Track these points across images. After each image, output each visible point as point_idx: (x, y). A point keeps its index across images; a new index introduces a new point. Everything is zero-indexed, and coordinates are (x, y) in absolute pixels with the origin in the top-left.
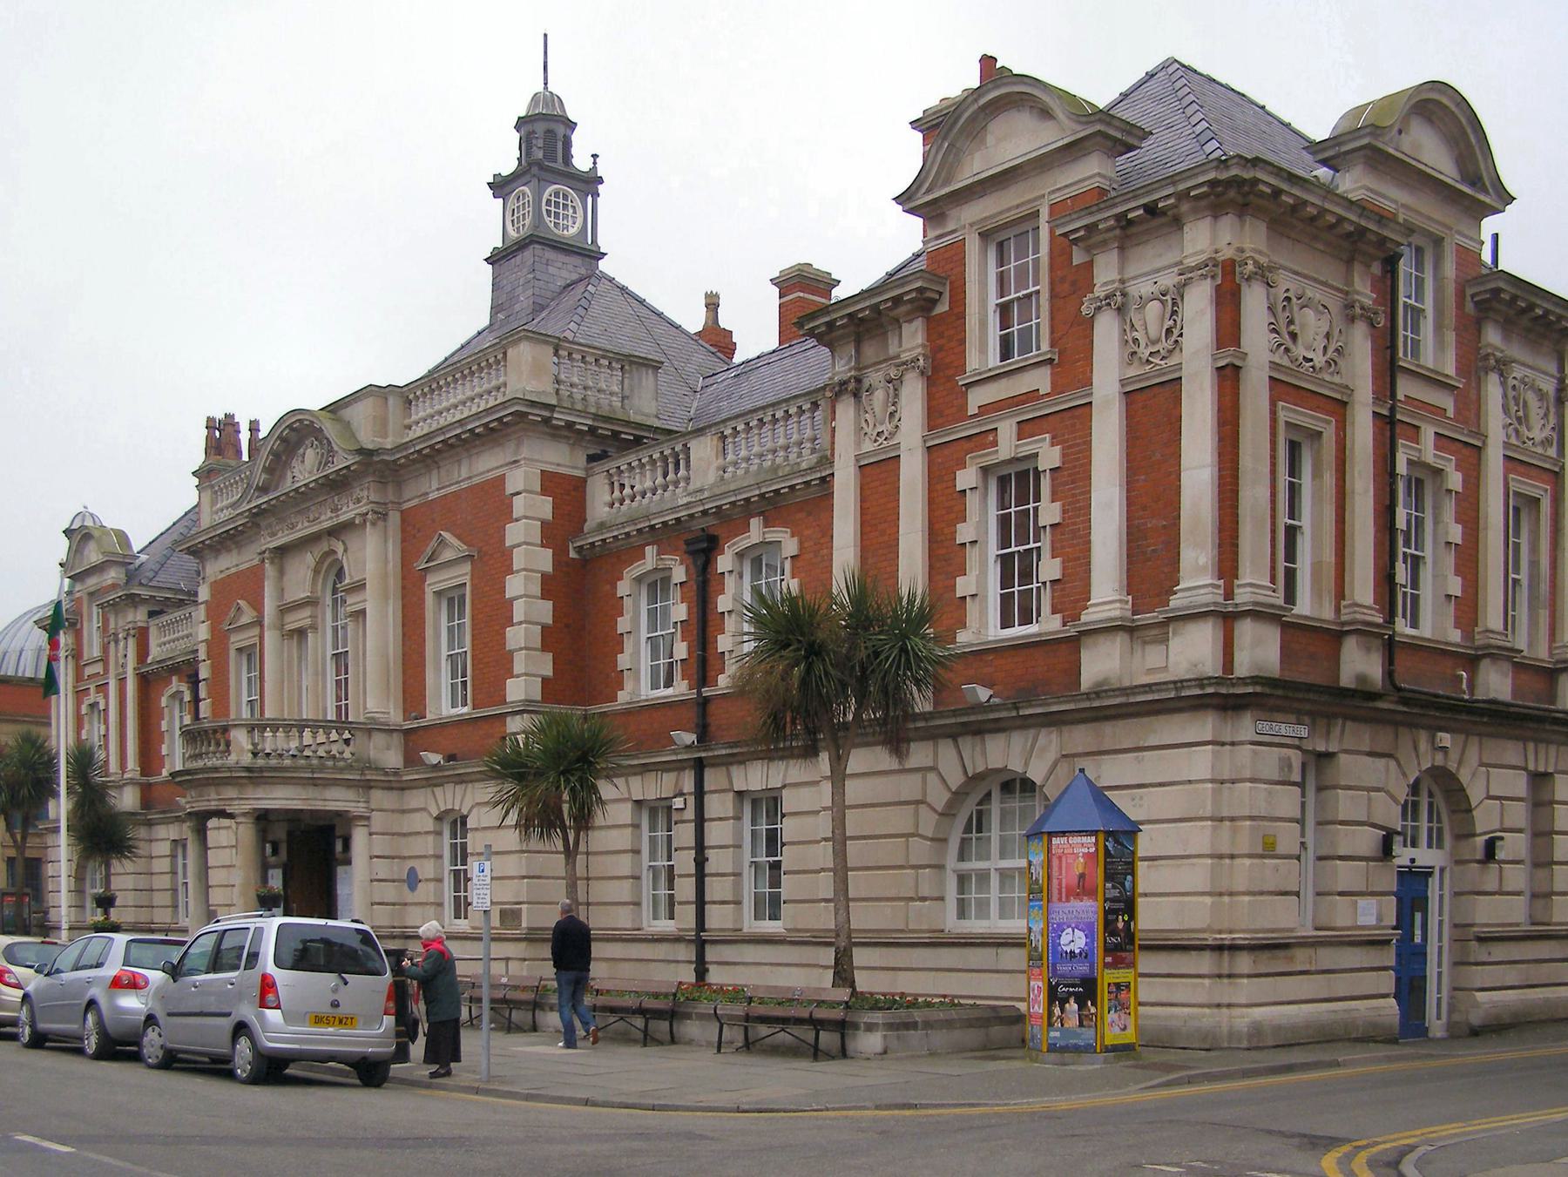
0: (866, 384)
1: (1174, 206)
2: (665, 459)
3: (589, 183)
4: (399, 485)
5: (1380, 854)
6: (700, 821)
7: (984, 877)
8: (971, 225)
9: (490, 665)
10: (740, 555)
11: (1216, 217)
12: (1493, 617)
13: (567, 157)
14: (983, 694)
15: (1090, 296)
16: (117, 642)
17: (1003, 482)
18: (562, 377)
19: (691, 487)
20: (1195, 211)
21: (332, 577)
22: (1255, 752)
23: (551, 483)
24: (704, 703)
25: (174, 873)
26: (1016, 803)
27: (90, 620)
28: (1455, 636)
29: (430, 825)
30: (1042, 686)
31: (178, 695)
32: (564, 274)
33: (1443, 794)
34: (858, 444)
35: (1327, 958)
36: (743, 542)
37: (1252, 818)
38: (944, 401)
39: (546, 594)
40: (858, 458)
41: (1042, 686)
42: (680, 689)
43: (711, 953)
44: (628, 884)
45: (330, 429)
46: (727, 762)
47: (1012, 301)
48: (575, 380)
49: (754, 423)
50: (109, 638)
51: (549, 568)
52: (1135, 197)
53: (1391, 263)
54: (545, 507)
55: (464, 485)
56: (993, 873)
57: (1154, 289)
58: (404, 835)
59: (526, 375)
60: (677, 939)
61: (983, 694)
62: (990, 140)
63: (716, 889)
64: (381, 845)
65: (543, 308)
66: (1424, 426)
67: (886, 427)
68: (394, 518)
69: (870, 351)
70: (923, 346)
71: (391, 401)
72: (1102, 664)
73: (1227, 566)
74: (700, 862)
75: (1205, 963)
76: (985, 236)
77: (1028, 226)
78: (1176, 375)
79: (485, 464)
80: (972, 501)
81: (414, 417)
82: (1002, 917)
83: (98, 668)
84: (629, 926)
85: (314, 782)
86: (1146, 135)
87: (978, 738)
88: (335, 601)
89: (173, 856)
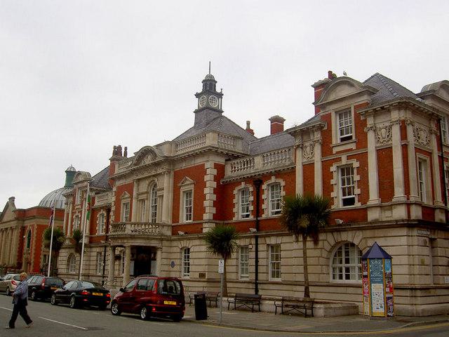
3: (220, 95)
4: (174, 165)
9: (199, 210)
10: (268, 185)
13: (215, 89)
14: (341, 222)
17: (343, 170)
24: (258, 222)
29: (179, 250)
35: (439, 292)
38: (73, 209)
41: (356, 219)
42: (251, 218)
43: (259, 287)
44: (179, 260)
45: (157, 151)
53: (439, 121)
54: (215, 172)
59: (211, 140)
60: (249, 283)
61: (341, 222)
63: (261, 269)
67: (310, 156)
68: (172, 173)
69: (305, 138)
72: (372, 215)
73: (407, 191)
74: (257, 262)
75: (408, 293)
77: (348, 111)
79: (199, 161)
80: (335, 174)
85: (148, 239)
86: (378, 91)
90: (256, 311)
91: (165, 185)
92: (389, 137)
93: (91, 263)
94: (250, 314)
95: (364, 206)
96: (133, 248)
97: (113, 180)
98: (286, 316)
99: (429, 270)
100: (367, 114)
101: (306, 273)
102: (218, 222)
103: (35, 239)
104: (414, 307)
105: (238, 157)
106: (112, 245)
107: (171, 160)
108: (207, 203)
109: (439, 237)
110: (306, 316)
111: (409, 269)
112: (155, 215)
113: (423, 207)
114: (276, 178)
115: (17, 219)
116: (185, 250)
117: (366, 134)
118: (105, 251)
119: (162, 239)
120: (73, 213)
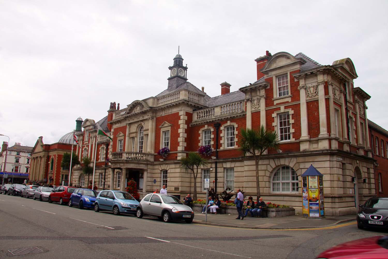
0: (253, 99)
1: (316, 73)
2: (204, 112)
3: (186, 69)
4: (156, 113)
5: (352, 181)
6: (216, 173)
7: (278, 184)
8: (274, 75)
10: (203, 131)
11: (323, 75)
12: (361, 142)
13: (182, 64)
15: (299, 86)
16: (92, 138)
18: (189, 97)
19: (215, 115)
20: (320, 74)
21: (140, 128)
22: (336, 163)
23: (187, 114)
24: (217, 152)
25: (99, 178)
26: (285, 171)
27: (86, 134)
28: (356, 144)
29: (159, 172)
30: (292, 150)
31: (103, 148)
32: (181, 82)
33: (357, 170)
34: (251, 109)
36: (226, 125)
37: (337, 174)
38: (83, 143)
39: (186, 132)
40: (251, 111)
41: (292, 150)
45: (144, 104)
46: (222, 162)
47: (281, 87)
48: (191, 97)
49: (228, 105)
50: (90, 137)
52: (309, 71)
54: (186, 118)
55: (170, 114)
56: (281, 183)
57: (312, 86)
58: (153, 173)
59: (183, 96)
61: (281, 151)
62: (277, 62)
64: (149, 175)
66: (350, 110)
67: (257, 106)
68: (155, 119)
70: (265, 94)
71: (155, 99)
72: (304, 147)
73: (329, 131)
76: (276, 77)
78: (318, 99)
79: (174, 110)
81: (159, 102)
82: (283, 191)
83: (87, 143)
84: (200, 191)
86: (306, 62)
87: (278, 159)
88: (140, 132)
92: (317, 93)
95: (298, 141)
96: (128, 169)
97: (112, 124)
99: (341, 184)
100: (299, 78)
101: (258, 187)
102: (187, 152)
103: (56, 164)
105: (201, 108)
106: (112, 167)
108: (180, 139)
109: (347, 162)
111: (331, 184)
112: (141, 148)
113: (338, 142)
114: (231, 122)
115: (44, 151)
116: (164, 172)
117: (299, 92)
118: (105, 172)
119: (147, 163)
120: (83, 147)
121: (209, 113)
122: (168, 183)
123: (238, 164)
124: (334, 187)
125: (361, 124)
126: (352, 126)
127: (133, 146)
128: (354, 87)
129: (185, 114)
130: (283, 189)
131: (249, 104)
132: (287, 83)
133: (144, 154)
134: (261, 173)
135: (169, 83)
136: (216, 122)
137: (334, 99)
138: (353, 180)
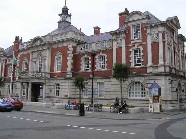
0: (117, 39)
3: (70, 16)
6: (92, 85)
7: (133, 93)
9: (64, 67)
12: (181, 68)
14: (135, 73)
23: (73, 47)
24: (93, 72)
25: (8, 89)
26: (138, 84)
29: (54, 85)
30: (142, 72)
41: (142, 72)
42: (90, 70)
51: (73, 56)
64: (47, 87)
65: (65, 28)
68: (51, 49)
72: (149, 70)
73: (164, 61)
79: (65, 44)
85: (39, 79)
89: (8, 87)
90: (100, 111)
91: (47, 55)
92: (158, 38)
93: (5, 90)
94: (98, 112)
98: (115, 113)
99: (170, 93)
104: (167, 108)
105: (82, 44)
107: (51, 43)
110: (99, 111)
112: (41, 68)
121: (86, 47)
122: (60, 92)
123: (107, 80)
124: (167, 94)
125: (182, 56)
126: (176, 58)
127: (35, 67)
128: (179, 34)
129: (72, 47)
130: (136, 96)
131: (115, 43)
132: (139, 31)
133: (44, 73)
134: (123, 86)
135: (59, 25)
136: (93, 53)
137: (168, 41)
138: (177, 90)
